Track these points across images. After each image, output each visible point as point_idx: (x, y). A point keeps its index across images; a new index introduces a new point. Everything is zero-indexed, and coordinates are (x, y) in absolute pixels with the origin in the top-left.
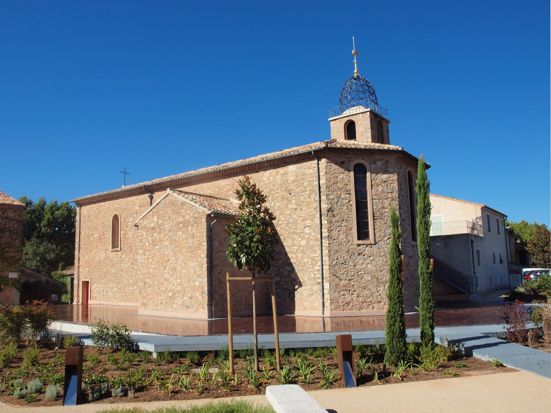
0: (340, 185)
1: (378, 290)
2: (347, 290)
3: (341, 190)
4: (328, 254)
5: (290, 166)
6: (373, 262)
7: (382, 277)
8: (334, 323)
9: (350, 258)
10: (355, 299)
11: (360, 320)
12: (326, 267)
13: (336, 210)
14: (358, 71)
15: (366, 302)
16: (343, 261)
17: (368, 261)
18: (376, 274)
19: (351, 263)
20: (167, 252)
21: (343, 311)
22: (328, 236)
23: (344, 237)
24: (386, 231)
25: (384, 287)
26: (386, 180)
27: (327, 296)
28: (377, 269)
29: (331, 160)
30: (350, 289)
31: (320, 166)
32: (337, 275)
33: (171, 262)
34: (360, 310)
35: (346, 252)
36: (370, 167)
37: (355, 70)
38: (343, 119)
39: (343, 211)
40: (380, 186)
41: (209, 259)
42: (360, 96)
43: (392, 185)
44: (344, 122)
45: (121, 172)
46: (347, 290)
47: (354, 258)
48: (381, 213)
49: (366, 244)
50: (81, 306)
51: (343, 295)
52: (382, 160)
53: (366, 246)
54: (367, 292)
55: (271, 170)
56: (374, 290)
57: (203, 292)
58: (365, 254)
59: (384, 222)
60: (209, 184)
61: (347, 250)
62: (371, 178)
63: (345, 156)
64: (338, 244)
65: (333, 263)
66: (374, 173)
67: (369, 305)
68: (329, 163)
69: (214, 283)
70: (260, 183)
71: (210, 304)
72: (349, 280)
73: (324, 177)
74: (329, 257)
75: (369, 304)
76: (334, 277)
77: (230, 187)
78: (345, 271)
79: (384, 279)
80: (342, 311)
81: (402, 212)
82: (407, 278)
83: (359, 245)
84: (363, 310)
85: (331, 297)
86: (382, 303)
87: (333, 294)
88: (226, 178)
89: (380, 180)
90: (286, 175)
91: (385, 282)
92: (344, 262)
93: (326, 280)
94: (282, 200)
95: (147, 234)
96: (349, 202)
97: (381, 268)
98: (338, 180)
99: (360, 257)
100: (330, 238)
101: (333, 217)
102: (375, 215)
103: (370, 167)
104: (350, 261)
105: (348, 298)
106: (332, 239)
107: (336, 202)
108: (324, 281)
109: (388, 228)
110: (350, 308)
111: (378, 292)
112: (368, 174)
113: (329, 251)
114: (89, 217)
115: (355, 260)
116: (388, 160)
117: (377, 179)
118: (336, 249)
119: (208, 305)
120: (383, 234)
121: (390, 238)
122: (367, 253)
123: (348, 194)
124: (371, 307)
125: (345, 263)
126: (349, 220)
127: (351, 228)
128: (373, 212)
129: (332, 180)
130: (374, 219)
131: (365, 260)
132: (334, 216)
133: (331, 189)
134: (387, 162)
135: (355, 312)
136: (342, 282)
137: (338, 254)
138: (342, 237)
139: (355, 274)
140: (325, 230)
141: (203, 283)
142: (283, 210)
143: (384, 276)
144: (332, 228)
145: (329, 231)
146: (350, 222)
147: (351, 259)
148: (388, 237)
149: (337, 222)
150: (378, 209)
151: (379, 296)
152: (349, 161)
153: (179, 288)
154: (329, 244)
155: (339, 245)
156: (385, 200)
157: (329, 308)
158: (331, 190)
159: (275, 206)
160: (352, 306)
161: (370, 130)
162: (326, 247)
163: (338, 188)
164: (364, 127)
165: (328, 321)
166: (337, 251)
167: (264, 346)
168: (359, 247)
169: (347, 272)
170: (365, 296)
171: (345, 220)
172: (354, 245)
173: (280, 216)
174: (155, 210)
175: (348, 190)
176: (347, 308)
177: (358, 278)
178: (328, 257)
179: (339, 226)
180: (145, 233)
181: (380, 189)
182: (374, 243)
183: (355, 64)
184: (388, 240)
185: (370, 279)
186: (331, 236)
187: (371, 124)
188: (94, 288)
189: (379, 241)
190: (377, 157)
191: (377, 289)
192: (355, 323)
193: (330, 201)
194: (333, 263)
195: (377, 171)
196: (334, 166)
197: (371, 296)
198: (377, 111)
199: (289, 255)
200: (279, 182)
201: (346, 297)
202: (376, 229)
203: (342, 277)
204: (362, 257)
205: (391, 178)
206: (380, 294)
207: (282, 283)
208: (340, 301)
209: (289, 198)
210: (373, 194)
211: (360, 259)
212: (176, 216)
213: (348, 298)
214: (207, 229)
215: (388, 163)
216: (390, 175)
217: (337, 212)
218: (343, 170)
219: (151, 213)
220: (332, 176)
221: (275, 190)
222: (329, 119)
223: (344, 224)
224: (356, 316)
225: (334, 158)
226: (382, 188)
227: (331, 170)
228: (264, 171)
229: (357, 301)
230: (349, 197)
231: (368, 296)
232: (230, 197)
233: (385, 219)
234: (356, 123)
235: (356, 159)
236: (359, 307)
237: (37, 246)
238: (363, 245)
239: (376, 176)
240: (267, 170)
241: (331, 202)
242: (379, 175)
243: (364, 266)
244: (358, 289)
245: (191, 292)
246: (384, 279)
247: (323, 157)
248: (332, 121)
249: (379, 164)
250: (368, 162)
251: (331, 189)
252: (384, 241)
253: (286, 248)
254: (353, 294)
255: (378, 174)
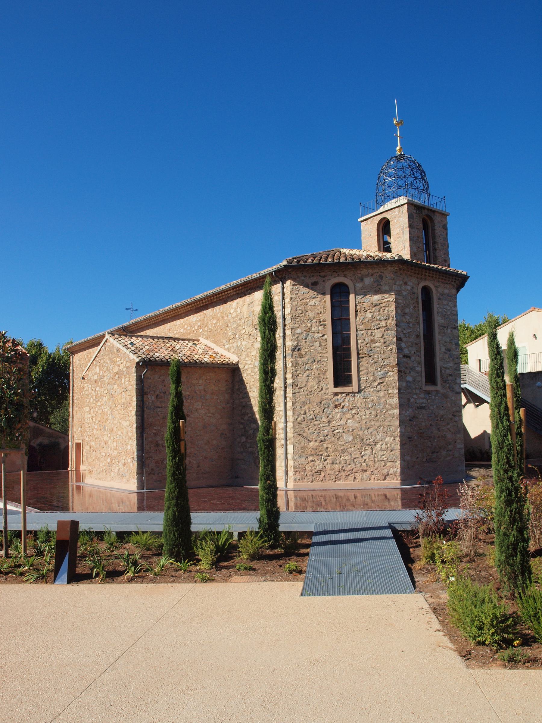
0: (311, 314)
1: (362, 454)
2: (318, 455)
3: (312, 321)
4: (293, 408)
5: (256, 293)
6: (356, 416)
7: (369, 437)
8: (299, 499)
9: (323, 412)
10: (329, 466)
11: (336, 495)
12: (290, 425)
13: (304, 347)
14: (401, 148)
15: (344, 471)
16: (312, 416)
17: (348, 416)
18: (360, 433)
19: (324, 419)
20: (106, 410)
21: (312, 482)
22: (293, 383)
23: (315, 384)
24: (376, 373)
25: (371, 451)
26: (379, 302)
27: (291, 463)
28: (361, 425)
29: (298, 281)
30: (321, 453)
31: (285, 290)
32: (304, 435)
33: (109, 421)
34: (335, 481)
35: (317, 403)
36: (355, 286)
37: (398, 146)
38: (375, 217)
39: (314, 349)
40: (368, 311)
41: (140, 417)
42: (399, 183)
43: (387, 309)
44: (377, 222)
45: (126, 309)
46: (318, 455)
47: (328, 412)
48: (370, 349)
49: (345, 393)
50: (75, 471)
51: (312, 461)
52: (372, 275)
53: (347, 395)
54: (346, 458)
55: (238, 299)
56: (356, 454)
57: (133, 458)
58: (344, 405)
59: (373, 361)
60: (182, 320)
61: (319, 401)
62: (356, 301)
63: (319, 274)
64: (306, 393)
65: (299, 419)
66: (361, 295)
67: (349, 474)
68: (296, 285)
69: (146, 447)
70: (228, 316)
71: (140, 473)
72: (321, 441)
73: (289, 306)
74: (293, 411)
75: (349, 473)
76: (300, 438)
77: (200, 324)
78: (316, 430)
79: (372, 440)
80: (310, 483)
81: (403, 345)
82: (409, 438)
83: (336, 394)
84: (341, 482)
85: (296, 464)
86: (368, 472)
87: (298, 460)
88: (197, 312)
89: (369, 304)
90: (252, 304)
91: (373, 444)
92: (314, 418)
93: (290, 441)
94: (248, 337)
95: (91, 388)
96: (323, 336)
97: (367, 424)
98: (308, 308)
99: (337, 410)
100: (294, 386)
101: (300, 358)
102: (361, 352)
103: (355, 286)
104: (323, 416)
105: (319, 465)
106: (298, 387)
107: (304, 337)
108: (288, 443)
109: (379, 369)
110: (321, 478)
111: (362, 457)
112: (352, 297)
113: (294, 404)
114: (80, 366)
115: (330, 414)
116: (382, 274)
117: (364, 302)
118: (304, 400)
119: (137, 474)
120: (371, 378)
121: (382, 383)
122: (347, 404)
123: (321, 325)
124: (351, 477)
125: (316, 418)
126: (323, 361)
127: (326, 371)
128: (357, 348)
129: (299, 309)
130: (358, 358)
131: (344, 414)
132: (301, 356)
133: (297, 320)
134: (381, 277)
135: (329, 484)
136: (311, 444)
137: (307, 407)
138: (312, 383)
139: (330, 433)
140: (289, 376)
141: (133, 447)
142: (249, 351)
143: (371, 436)
144: (298, 372)
145: (294, 377)
146: (323, 363)
147: (324, 413)
148: (379, 381)
149: (306, 364)
150: (365, 343)
151: (364, 462)
152: (324, 281)
153: (115, 453)
154: (293, 393)
155: (308, 395)
156: (376, 331)
157: (293, 478)
158: (298, 322)
159: (241, 346)
160: (325, 476)
161: (408, 229)
162: (290, 398)
163: (308, 318)
164: (400, 226)
165: (291, 495)
166: (304, 403)
167: (92, 528)
168: (336, 397)
169: (318, 431)
170: (343, 462)
171: (316, 361)
172: (329, 394)
173: (246, 359)
174: (97, 360)
175: (322, 320)
176: (318, 478)
177: (333, 438)
178: (292, 411)
179: (308, 370)
180: (90, 386)
181: (369, 315)
182: (357, 391)
183: (398, 138)
184: (379, 387)
185: (350, 440)
186: (297, 383)
187: (409, 221)
188: (85, 449)
189: (365, 388)
190: (365, 271)
191: (361, 453)
192: (327, 499)
193: (296, 336)
194: (299, 419)
195: (366, 291)
196: (303, 290)
197: (352, 463)
198: (422, 200)
199: (254, 409)
200: (246, 314)
201: (316, 464)
202: (361, 371)
203: (311, 437)
204: (340, 410)
205: (385, 300)
206: (365, 460)
207: (248, 446)
208: (307, 469)
209: (255, 335)
210: (358, 323)
211: (337, 414)
212: (113, 366)
213: (318, 465)
214: (137, 380)
215: (382, 279)
216: (384, 295)
217: (306, 350)
218: (316, 293)
219: (94, 362)
220: (300, 303)
221: (242, 325)
222: (359, 220)
223: (315, 366)
224: (324, 490)
225: (303, 278)
226: (372, 314)
227: (299, 294)
228: (232, 300)
229: (331, 469)
230: (323, 330)
231: (348, 463)
232: (200, 336)
233: (376, 356)
234: (392, 221)
235: (335, 277)
236: (334, 477)
237: (241, 392)
238: (342, 393)
239: (363, 299)
240: (234, 300)
241: (297, 338)
242: (367, 297)
243: (343, 422)
244: (333, 454)
245: (124, 458)
246: (372, 440)
247: (288, 279)
248: (362, 221)
249: (368, 281)
250: (351, 280)
251: (297, 320)
252: (373, 387)
253: (252, 400)
254: (326, 460)
255: (366, 295)
